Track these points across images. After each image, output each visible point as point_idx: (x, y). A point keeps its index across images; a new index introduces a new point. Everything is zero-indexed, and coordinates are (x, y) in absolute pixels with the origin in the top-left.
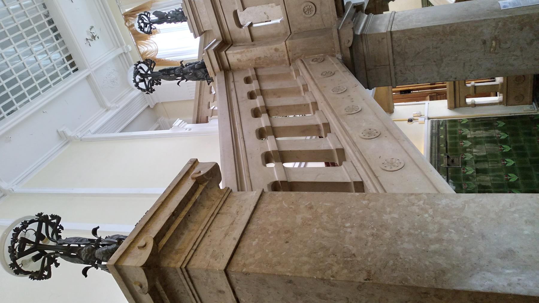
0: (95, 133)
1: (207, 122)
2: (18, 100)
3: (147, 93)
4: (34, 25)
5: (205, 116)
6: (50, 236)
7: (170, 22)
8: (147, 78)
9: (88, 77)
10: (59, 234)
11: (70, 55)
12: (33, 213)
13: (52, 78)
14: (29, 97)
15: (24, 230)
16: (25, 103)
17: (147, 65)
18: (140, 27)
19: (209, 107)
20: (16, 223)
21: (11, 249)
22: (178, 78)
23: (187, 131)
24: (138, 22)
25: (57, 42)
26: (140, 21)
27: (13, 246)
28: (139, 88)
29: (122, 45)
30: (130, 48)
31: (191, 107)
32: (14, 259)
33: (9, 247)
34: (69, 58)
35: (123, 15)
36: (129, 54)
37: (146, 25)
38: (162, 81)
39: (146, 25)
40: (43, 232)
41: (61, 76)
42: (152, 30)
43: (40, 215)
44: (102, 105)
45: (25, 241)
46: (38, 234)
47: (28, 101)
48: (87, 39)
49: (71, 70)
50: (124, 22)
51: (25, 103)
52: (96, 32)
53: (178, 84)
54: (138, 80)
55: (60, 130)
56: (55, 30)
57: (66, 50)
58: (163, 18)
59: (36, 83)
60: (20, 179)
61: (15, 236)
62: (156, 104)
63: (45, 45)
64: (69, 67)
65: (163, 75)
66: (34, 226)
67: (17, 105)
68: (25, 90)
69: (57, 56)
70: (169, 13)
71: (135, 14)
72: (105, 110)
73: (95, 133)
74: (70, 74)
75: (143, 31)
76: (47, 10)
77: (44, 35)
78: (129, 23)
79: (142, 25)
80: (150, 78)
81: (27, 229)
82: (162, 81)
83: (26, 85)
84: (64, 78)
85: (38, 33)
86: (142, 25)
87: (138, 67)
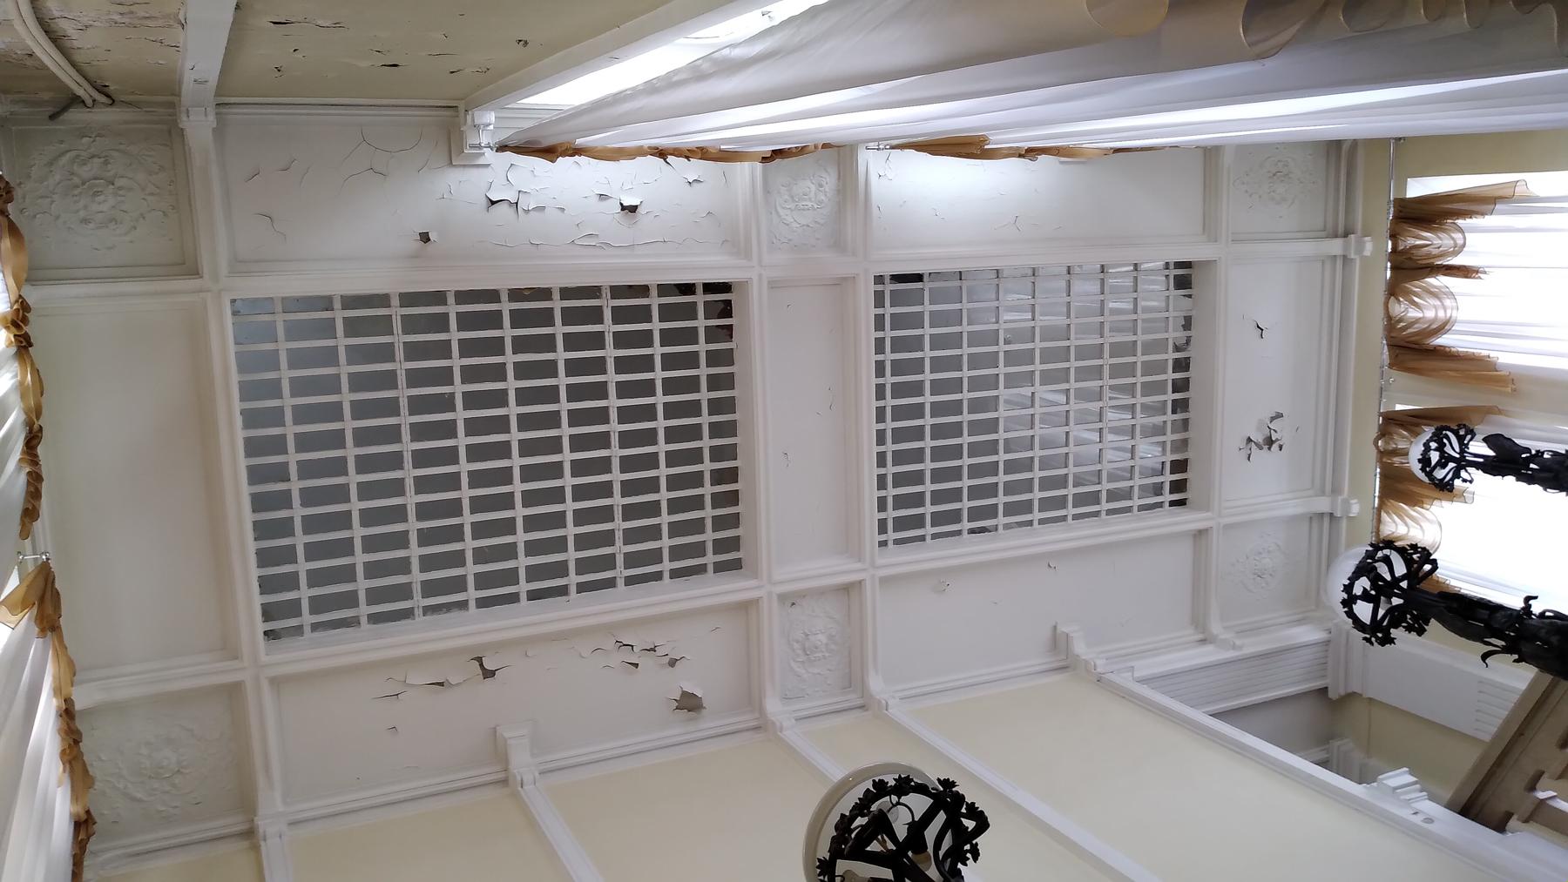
0: (1142, 681)
1: (1500, 827)
2: (1011, 509)
3: (1368, 640)
4: (1140, 358)
5: (1502, 807)
6: (941, 853)
7: (1530, 479)
8: (1389, 598)
9: (1200, 534)
10: (960, 866)
11: (1186, 460)
12: (933, 774)
13: (1113, 496)
14: (1037, 515)
15: (895, 798)
16: (1020, 524)
17: (1408, 562)
18: (1425, 461)
19: (1532, 787)
20: (888, 767)
21: (844, 824)
22: (1493, 641)
23: (1417, 819)
24: (1427, 446)
25: (1170, 417)
26: (1433, 445)
27: (852, 818)
28: (1351, 614)
29: (1336, 491)
30: (1355, 509)
31: (1464, 764)
32: (836, 852)
33: (843, 816)
34: (1180, 466)
35: (1381, 414)
36: (1344, 524)
37: (1445, 460)
38: (1434, 626)
39: (1445, 460)
40: (930, 834)
41: (1136, 502)
42: (1457, 482)
43: (948, 784)
44: (1199, 621)
45: (881, 824)
46: (917, 828)
47: (1030, 523)
48: (1249, 440)
49: (1168, 497)
50: (1374, 433)
51: (1020, 524)
52: (1282, 431)
53: (1485, 657)
54: (1357, 590)
55: (1062, 629)
56: (1181, 386)
57: (1183, 444)
58: (1509, 460)
59: (1071, 491)
60: (913, 692)
61: (869, 798)
62: (1351, 696)
63: (1110, 437)
64: (1167, 487)
65: (1450, 610)
66: (919, 803)
67: (1002, 520)
68: (1037, 495)
69: (1150, 453)
70: (1540, 453)
71: (1418, 425)
72: (1201, 636)
73: (1142, 681)
74: (1160, 505)
75: (1429, 475)
76: (1188, 333)
77: (1149, 389)
78: (1386, 443)
79: (1435, 457)
80: (1396, 601)
81: (904, 799)
82: (1434, 626)
83: (1046, 484)
84: (1142, 508)
85: (1140, 379)
86: (1435, 457)
87: (1380, 554)
